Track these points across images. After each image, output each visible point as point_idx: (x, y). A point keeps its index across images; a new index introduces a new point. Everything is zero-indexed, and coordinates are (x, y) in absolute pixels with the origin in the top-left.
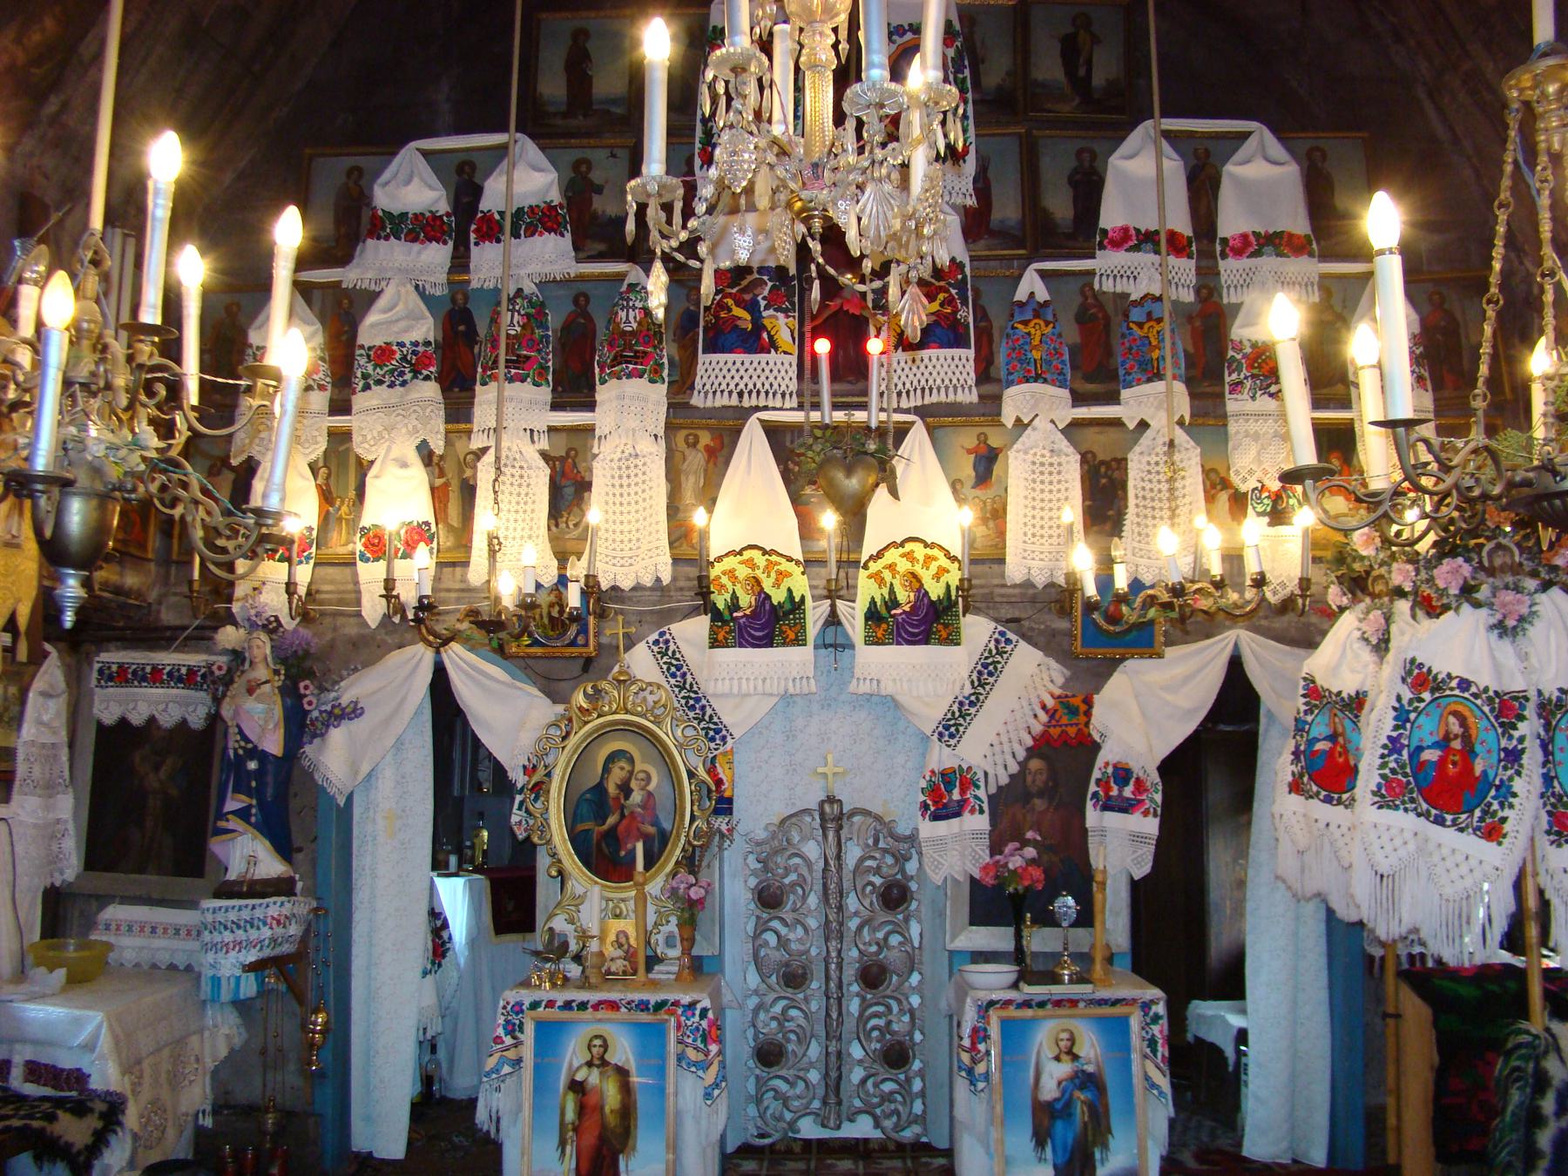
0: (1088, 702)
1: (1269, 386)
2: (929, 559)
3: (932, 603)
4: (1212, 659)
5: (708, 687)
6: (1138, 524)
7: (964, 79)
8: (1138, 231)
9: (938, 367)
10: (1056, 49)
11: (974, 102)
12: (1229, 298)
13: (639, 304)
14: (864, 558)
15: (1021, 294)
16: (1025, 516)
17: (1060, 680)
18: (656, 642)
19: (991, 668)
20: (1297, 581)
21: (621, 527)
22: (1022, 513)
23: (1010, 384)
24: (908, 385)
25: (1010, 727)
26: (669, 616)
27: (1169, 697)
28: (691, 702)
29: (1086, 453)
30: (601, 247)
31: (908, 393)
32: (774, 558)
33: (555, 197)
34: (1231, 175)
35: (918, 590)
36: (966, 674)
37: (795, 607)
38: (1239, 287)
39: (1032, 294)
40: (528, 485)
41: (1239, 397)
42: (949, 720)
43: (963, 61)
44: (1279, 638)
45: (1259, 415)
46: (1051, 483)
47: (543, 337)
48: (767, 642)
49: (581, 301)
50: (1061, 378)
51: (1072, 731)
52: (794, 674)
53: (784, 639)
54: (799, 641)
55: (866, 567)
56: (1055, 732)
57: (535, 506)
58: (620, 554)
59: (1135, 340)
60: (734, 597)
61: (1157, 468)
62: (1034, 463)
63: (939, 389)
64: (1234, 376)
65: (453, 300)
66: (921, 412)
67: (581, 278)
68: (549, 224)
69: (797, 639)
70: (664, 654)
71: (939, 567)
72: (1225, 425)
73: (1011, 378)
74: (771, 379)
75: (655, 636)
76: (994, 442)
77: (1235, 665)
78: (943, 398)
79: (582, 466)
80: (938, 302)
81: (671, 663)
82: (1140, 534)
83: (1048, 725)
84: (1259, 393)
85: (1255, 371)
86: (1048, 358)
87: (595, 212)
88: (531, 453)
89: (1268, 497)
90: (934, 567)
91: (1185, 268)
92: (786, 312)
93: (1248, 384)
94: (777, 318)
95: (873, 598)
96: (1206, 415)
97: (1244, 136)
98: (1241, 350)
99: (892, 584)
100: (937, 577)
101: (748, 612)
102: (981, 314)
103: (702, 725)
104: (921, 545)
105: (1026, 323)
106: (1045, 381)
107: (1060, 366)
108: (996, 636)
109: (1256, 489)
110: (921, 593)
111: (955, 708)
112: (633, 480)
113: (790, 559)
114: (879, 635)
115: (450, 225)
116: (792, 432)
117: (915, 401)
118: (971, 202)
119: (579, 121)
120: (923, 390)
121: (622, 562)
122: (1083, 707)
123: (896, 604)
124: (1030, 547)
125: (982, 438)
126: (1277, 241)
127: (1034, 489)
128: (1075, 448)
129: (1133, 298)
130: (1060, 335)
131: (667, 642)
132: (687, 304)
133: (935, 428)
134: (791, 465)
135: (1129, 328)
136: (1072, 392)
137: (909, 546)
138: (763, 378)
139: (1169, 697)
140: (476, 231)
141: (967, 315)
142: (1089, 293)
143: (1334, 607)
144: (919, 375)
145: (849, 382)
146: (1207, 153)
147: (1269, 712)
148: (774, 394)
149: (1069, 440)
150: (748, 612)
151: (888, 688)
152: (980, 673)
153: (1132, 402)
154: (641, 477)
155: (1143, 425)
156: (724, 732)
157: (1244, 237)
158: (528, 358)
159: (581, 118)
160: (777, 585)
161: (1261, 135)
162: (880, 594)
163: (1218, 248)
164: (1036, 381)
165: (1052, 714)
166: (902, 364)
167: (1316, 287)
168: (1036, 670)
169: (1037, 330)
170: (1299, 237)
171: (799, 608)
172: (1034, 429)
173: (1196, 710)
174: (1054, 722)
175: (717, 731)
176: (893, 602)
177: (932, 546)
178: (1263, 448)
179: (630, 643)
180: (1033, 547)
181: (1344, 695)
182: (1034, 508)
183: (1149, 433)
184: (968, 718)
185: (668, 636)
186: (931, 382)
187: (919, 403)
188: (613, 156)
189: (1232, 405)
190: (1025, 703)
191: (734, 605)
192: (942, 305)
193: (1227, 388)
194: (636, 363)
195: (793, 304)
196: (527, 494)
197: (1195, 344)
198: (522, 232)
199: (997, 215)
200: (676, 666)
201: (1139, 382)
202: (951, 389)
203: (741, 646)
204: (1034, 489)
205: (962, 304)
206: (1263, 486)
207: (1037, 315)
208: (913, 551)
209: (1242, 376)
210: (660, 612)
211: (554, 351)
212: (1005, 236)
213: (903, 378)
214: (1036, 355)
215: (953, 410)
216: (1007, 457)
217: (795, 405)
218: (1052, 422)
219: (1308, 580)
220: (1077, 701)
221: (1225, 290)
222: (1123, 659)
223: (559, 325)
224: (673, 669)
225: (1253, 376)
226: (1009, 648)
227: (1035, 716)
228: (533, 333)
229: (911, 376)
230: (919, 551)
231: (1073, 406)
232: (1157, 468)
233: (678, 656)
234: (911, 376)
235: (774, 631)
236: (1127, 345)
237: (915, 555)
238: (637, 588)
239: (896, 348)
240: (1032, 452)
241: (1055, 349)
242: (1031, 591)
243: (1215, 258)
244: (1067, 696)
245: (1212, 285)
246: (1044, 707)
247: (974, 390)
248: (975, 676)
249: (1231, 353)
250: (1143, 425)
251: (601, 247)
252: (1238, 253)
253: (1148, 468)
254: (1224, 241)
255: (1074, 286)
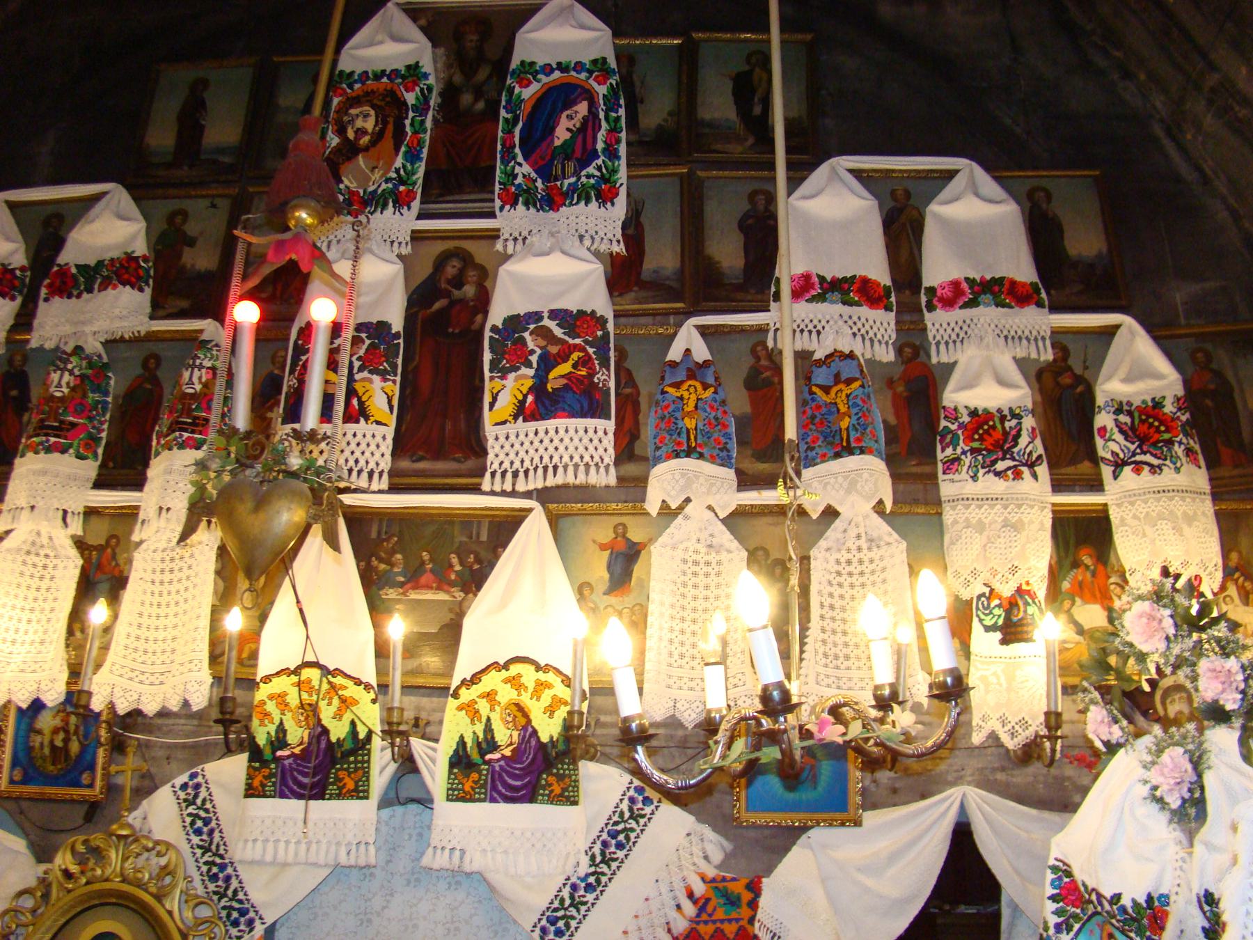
0: (755, 888)
1: (994, 462)
2: (541, 686)
3: (541, 746)
4: (935, 822)
5: (240, 851)
6: (824, 642)
7: (618, 119)
8: (822, 279)
9: (567, 440)
10: (729, 86)
11: (628, 144)
12: (938, 357)
13: (207, 363)
14: (455, 682)
15: (675, 353)
16: (672, 630)
17: (717, 857)
18: (184, 786)
19: (621, 837)
20: (1042, 718)
21: (156, 634)
22: (667, 626)
23: (657, 460)
24: (527, 464)
25: (643, 922)
26: (203, 753)
27: (869, 882)
28: (215, 870)
29: (756, 549)
30: (184, 304)
31: (526, 472)
32: (339, 680)
33: (140, 248)
34: (935, 215)
35: (525, 728)
36: (583, 845)
37: (359, 746)
38: (951, 345)
39: (688, 351)
40: (52, 578)
41: (956, 477)
42: (556, 910)
43: (618, 99)
44: (1020, 800)
45: (982, 500)
46: (707, 587)
47: (98, 402)
48: (318, 792)
49: (151, 364)
50: (725, 453)
51: (730, 929)
52: (350, 837)
53: (340, 789)
54: (360, 793)
55: (456, 695)
56: (706, 930)
57: (56, 605)
58: (150, 669)
59: (818, 407)
60: (281, 729)
61: (848, 569)
62: (685, 561)
63: (566, 467)
64: (949, 451)
65: (10, 361)
66: (544, 496)
67: (151, 337)
68: (126, 276)
69: (356, 790)
70: (190, 802)
71: (554, 697)
72: (940, 514)
73: (658, 453)
74: (358, 454)
75: (184, 778)
76: (635, 535)
77: (962, 836)
78: (570, 479)
79: (121, 558)
80: (571, 362)
81: (197, 816)
82: (826, 655)
83: (695, 921)
84: (982, 471)
85: (976, 445)
86: (707, 428)
87: (184, 267)
88: (63, 538)
89: (999, 606)
90: (547, 697)
91: (882, 322)
92: (383, 375)
93: (967, 460)
94: (370, 381)
95: (462, 737)
96: (916, 502)
97: (950, 175)
98: (956, 419)
99: (489, 719)
100: (550, 711)
101: (297, 751)
102: (625, 377)
103: (224, 902)
104: (532, 668)
105: (677, 385)
106: (701, 456)
107: (723, 440)
108: (632, 793)
109: (983, 595)
110: (528, 732)
111: (566, 893)
112: (177, 575)
113: (358, 682)
114: (467, 788)
115: (23, 280)
116: (381, 521)
117: (536, 483)
118: (619, 248)
119: (183, 173)
120: (545, 468)
121: (152, 679)
122: (747, 896)
123: (494, 746)
124: (677, 672)
125: (620, 530)
126: (996, 288)
127: (683, 596)
128: (741, 542)
129: (817, 356)
130: (723, 402)
131: (198, 786)
132: (271, 367)
133: (559, 516)
134: (375, 562)
135: (811, 393)
136: (739, 473)
137: (515, 669)
138: (347, 453)
139: (869, 882)
140: (49, 287)
141: (607, 379)
142: (762, 353)
143: (1098, 744)
144: (541, 451)
145: (455, 460)
146: (908, 194)
147: (1015, 908)
148: (360, 472)
149: (732, 532)
150: (297, 751)
151: (475, 862)
152: (605, 844)
153: (815, 484)
154: (186, 572)
155: (831, 514)
156: (252, 914)
157: (955, 284)
158: (73, 425)
159: (186, 168)
160: (338, 716)
161: (972, 171)
162: (471, 731)
163: (923, 299)
164: (688, 456)
165: (702, 904)
166: (522, 437)
167: (1048, 343)
168: (685, 842)
169: (691, 393)
170: (1024, 285)
171: (363, 748)
172: (687, 518)
173: (907, 901)
174: (704, 917)
175: (243, 912)
176: (488, 743)
177: (546, 668)
178: (989, 540)
179: (147, 786)
180: (680, 672)
181: (1126, 901)
182: (683, 620)
183: (838, 524)
184: (583, 908)
185: (200, 779)
186: (556, 459)
187: (540, 485)
188: (214, 206)
189: (948, 487)
190: (664, 888)
191: (280, 740)
192: (575, 366)
193: (940, 467)
194: (193, 432)
195: (394, 366)
196: (48, 589)
197: (897, 414)
198: (96, 286)
199: (650, 264)
200: (239, 910)
201: (824, 458)
202: (582, 468)
203: (283, 796)
204: (683, 596)
205: (601, 365)
206: (992, 591)
207: (691, 375)
208: (519, 676)
209: (959, 451)
210: (194, 746)
211: (111, 421)
212: (659, 288)
213: (522, 454)
214: (689, 423)
215: (584, 493)
216: (650, 552)
217: (385, 486)
218: (710, 508)
219: (1058, 715)
220: (738, 888)
221: (933, 348)
222: (804, 829)
223: (122, 390)
224: (199, 823)
225: (973, 451)
226: (648, 810)
227: (678, 907)
228: (85, 396)
229: (532, 452)
230: (529, 675)
231: (739, 490)
232: (848, 569)
233: (208, 806)
234: (532, 452)
235: (327, 777)
236: (810, 413)
237: (523, 680)
238: (163, 713)
239: (516, 417)
240: (681, 547)
241: (716, 418)
242: (680, 733)
243: (921, 311)
244: (724, 879)
245: (918, 343)
246: (690, 895)
247: (612, 470)
248: (597, 849)
249: (943, 423)
250: (831, 514)
251: (184, 304)
252: (948, 303)
253: (837, 568)
254: (931, 291)
255: (744, 345)
